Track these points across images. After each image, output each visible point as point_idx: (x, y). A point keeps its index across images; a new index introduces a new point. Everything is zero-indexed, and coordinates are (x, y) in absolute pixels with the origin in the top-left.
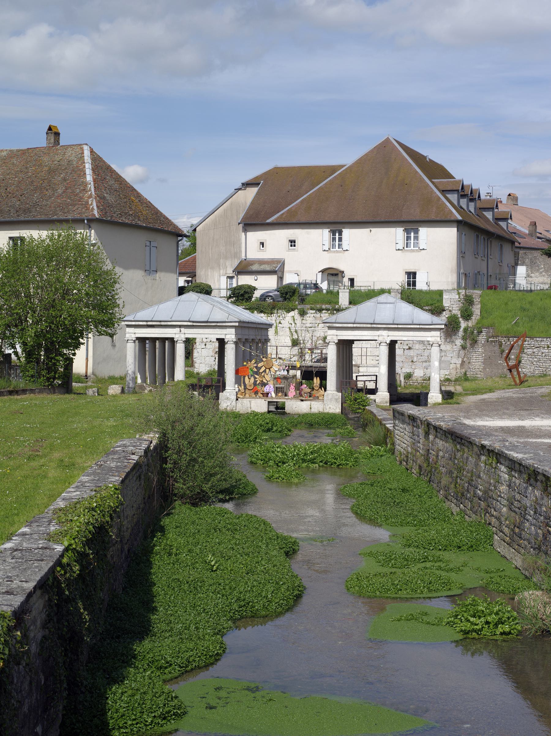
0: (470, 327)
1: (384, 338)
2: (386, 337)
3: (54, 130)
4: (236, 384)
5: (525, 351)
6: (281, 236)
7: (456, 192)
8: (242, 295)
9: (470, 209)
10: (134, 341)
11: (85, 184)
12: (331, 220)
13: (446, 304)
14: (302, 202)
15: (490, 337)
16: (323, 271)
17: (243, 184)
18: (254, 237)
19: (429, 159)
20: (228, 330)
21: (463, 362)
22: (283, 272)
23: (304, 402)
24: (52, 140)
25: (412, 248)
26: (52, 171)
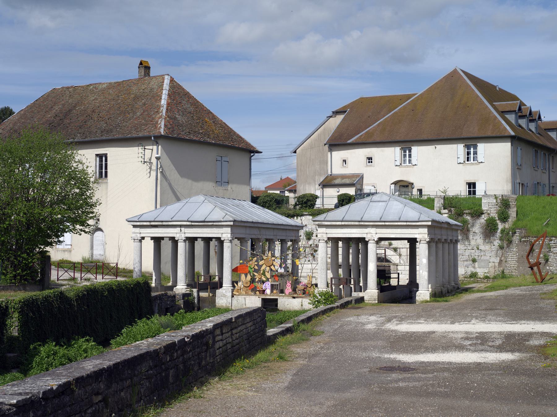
0: (507, 229)
1: (372, 236)
3: (144, 64)
5: (552, 249)
7: (514, 113)
8: (306, 203)
9: (530, 127)
10: (185, 241)
11: (159, 107)
12: (402, 139)
13: (484, 208)
14: (378, 125)
15: (522, 238)
16: (395, 183)
17: (333, 112)
18: (338, 155)
19: (499, 88)
21: (501, 261)
22: (362, 185)
23: (296, 299)
24: (143, 73)
26: (136, 98)
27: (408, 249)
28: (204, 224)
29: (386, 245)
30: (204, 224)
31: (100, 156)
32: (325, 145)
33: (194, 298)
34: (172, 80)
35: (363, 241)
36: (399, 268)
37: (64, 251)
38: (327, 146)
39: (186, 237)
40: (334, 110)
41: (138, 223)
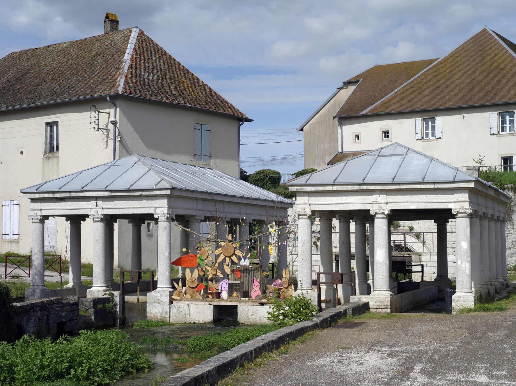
1: (381, 207)
2: (383, 205)
3: (111, 18)
4: (393, 271)
6: (376, 127)
12: (424, 108)
17: (344, 83)
18: (349, 130)
20: (158, 201)
25: (508, 132)
26: (98, 55)
27: (435, 235)
28: (129, 194)
29: (406, 230)
30: (129, 194)
31: (50, 125)
32: (334, 118)
33: (115, 305)
34: (141, 34)
35: (365, 217)
36: (423, 258)
37: (11, 242)
38: (336, 119)
39: (105, 215)
40: (345, 80)
41: (38, 196)
